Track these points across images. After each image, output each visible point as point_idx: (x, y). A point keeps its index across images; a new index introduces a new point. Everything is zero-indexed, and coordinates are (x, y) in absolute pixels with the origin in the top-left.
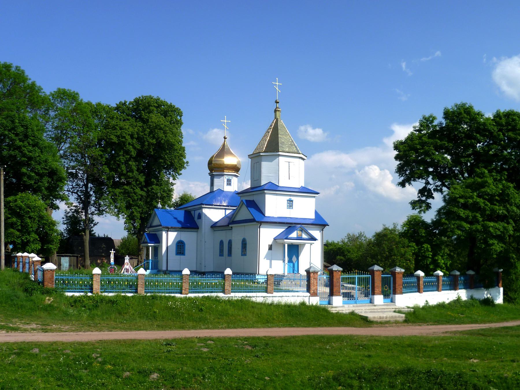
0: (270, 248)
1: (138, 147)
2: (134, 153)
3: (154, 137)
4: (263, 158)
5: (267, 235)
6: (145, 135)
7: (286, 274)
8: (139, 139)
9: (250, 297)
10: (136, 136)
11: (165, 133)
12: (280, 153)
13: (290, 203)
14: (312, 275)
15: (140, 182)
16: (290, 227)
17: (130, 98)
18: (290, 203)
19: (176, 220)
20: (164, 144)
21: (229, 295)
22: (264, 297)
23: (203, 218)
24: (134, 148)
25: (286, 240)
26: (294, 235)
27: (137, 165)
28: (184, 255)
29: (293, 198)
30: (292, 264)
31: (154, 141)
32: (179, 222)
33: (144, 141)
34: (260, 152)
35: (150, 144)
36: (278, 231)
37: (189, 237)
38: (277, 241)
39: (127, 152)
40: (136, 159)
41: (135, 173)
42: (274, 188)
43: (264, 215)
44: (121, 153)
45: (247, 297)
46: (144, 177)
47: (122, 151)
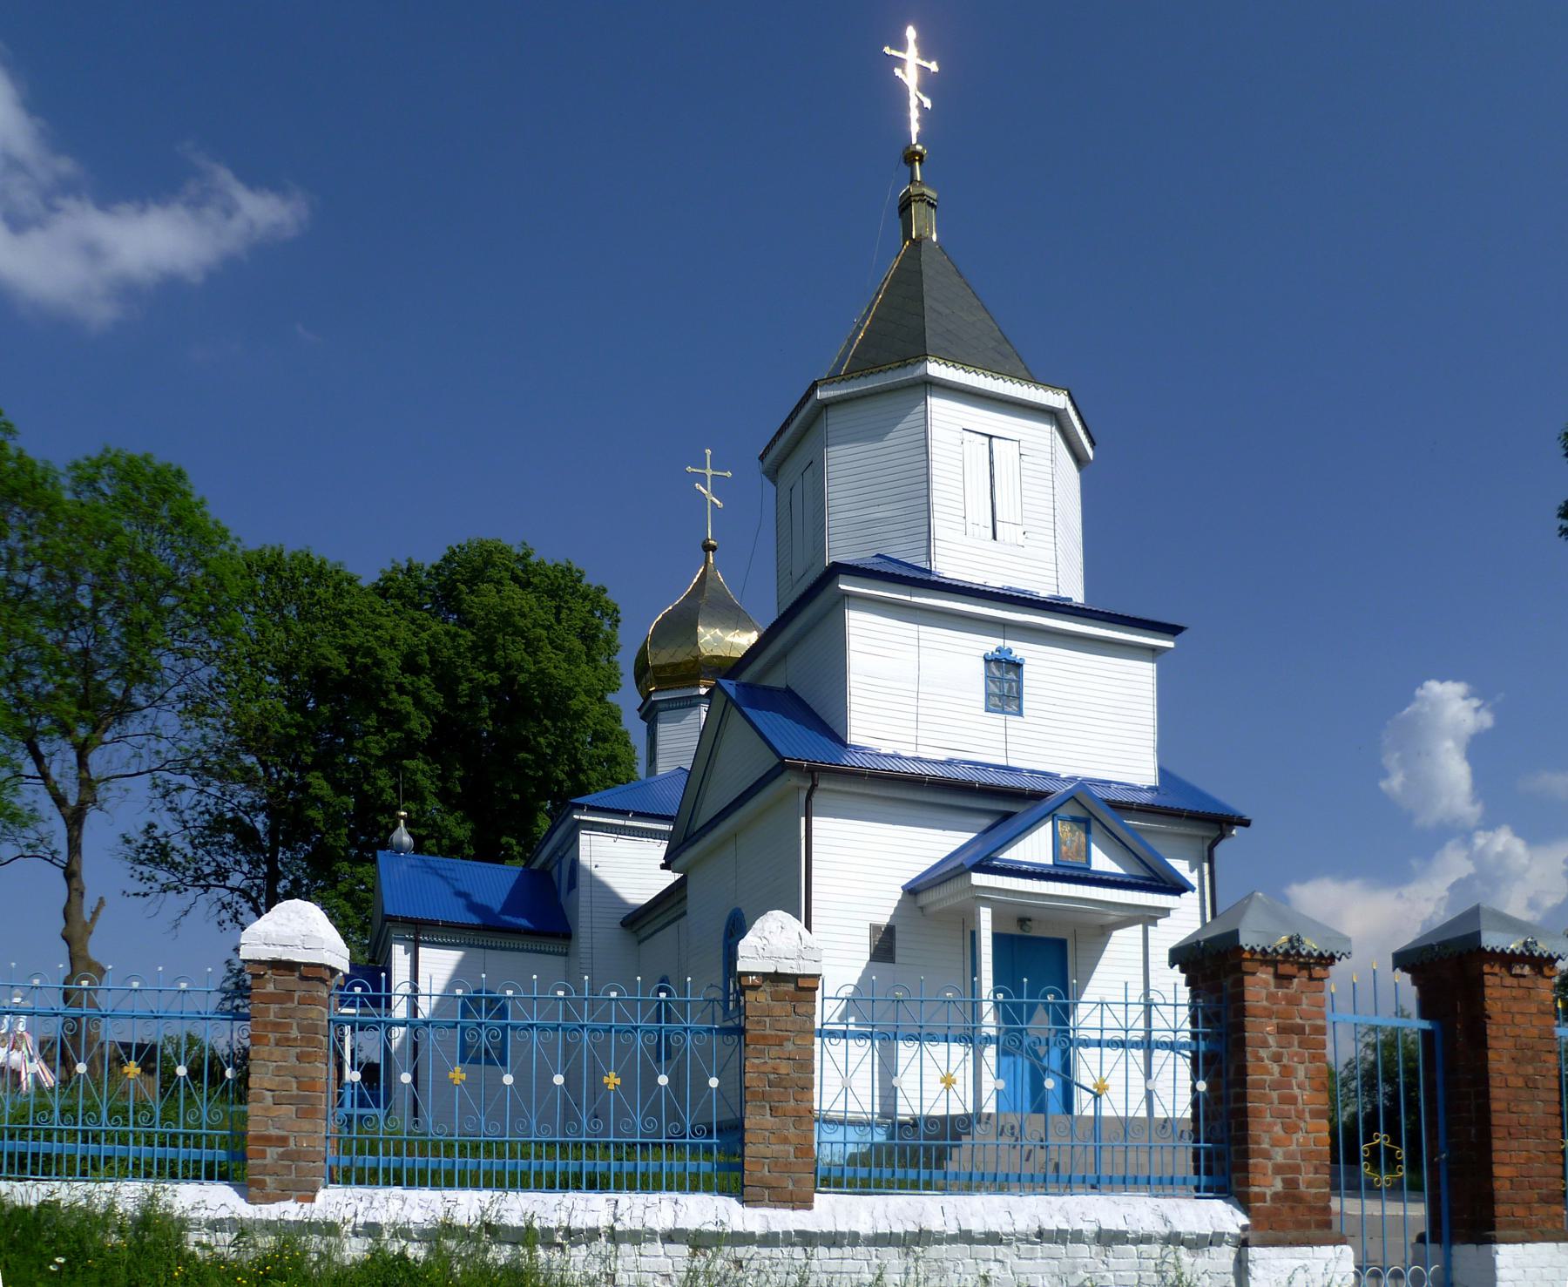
0: (885, 945)
1: (435, 699)
2: (420, 725)
3: (491, 666)
4: (834, 419)
5: (862, 866)
6: (459, 654)
7: (990, 1107)
8: (446, 680)
9: (527, 1236)
10: (425, 659)
11: (532, 647)
12: (935, 369)
13: (1005, 685)
14: (1259, 987)
15: (451, 838)
16: (1007, 816)
17: (429, 556)
18: (1005, 685)
19: (461, 902)
20: (525, 687)
21: (290, 1210)
22: (698, 1241)
23: (582, 880)
24: (418, 702)
25: (978, 879)
26: (1036, 847)
27: (440, 777)
28: (810, 1208)
29: (1020, 649)
30: (1024, 1065)
31: (495, 679)
32: (473, 907)
33: (458, 681)
34: (814, 386)
35: (477, 689)
36: (930, 844)
37: (524, 979)
38: (925, 899)
39: (394, 719)
40: (431, 750)
41: (433, 804)
42: (911, 584)
43: (836, 735)
44: (372, 721)
45: (494, 1231)
46: (469, 825)
47: (374, 716)
